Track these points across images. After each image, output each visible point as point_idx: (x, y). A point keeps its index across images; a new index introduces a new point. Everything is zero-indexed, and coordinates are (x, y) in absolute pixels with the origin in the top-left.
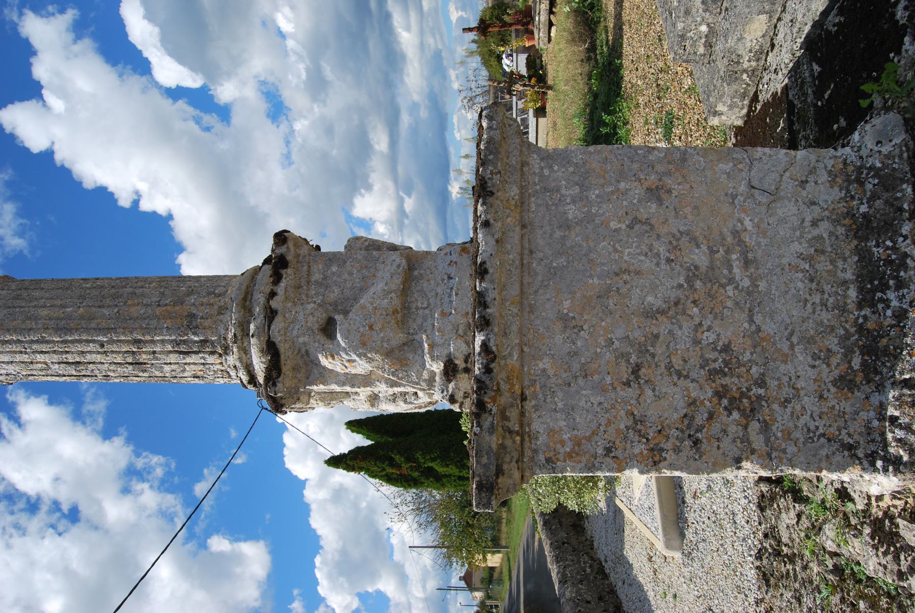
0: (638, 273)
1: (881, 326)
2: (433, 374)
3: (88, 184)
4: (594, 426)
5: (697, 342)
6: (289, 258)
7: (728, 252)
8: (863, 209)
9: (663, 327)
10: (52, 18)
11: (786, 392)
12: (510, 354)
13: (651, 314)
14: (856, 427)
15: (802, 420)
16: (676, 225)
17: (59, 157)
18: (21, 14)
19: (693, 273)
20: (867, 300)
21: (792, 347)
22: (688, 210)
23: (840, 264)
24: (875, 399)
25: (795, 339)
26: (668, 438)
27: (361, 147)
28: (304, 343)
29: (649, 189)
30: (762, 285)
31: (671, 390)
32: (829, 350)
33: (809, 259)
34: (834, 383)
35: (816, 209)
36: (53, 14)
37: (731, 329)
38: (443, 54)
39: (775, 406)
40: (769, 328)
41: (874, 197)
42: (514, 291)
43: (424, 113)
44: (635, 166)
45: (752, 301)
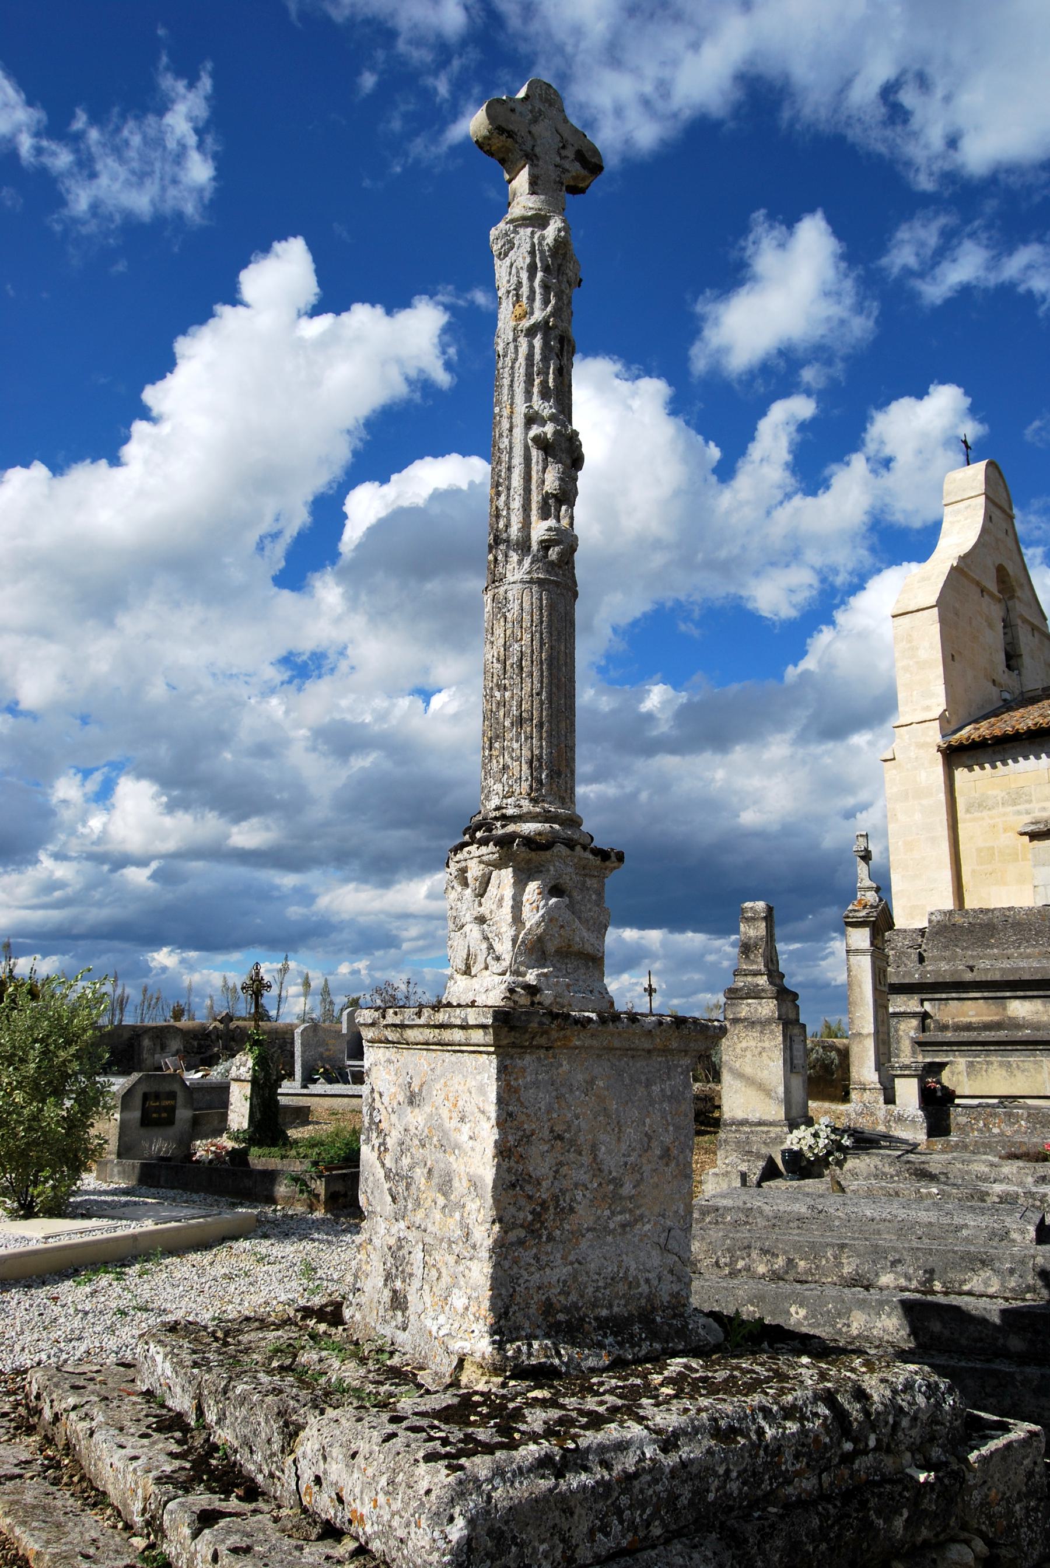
0: (619, 1139)
1: (589, 1333)
2: (524, 975)
3: (182, 346)
4: (527, 1104)
5: (576, 1185)
6: (607, 863)
7: (631, 1211)
8: (658, 1319)
9: (586, 1159)
10: (437, 351)
11: (544, 1258)
12: (579, 1039)
13: (594, 1148)
14: (520, 1318)
15: (524, 1273)
16: (647, 1168)
17: (226, 311)
18: (447, 307)
19: (618, 1183)
20: (603, 1324)
21: (572, 1263)
22: (656, 1179)
23: (623, 1302)
24: (538, 1332)
25: (576, 1265)
26: (517, 1162)
27: (238, 802)
28: (548, 870)
29: (668, 1149)
30: (609, 1239)
31: (547, 1165)
32: (569, 1294)
33: (625, 1278)
34: (548, 1299)
35: (656, 1283)
36: (444, 353)
37: (584, 1215)
38: (393, 951)
39: (534, 1250)
40: (584, 1244)
41: (670, 1326)
42: (616, 1044)
43: (295, 912)
44: (682, 1138)
45: (601, 1230)
